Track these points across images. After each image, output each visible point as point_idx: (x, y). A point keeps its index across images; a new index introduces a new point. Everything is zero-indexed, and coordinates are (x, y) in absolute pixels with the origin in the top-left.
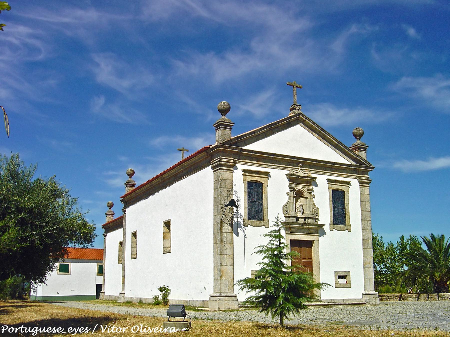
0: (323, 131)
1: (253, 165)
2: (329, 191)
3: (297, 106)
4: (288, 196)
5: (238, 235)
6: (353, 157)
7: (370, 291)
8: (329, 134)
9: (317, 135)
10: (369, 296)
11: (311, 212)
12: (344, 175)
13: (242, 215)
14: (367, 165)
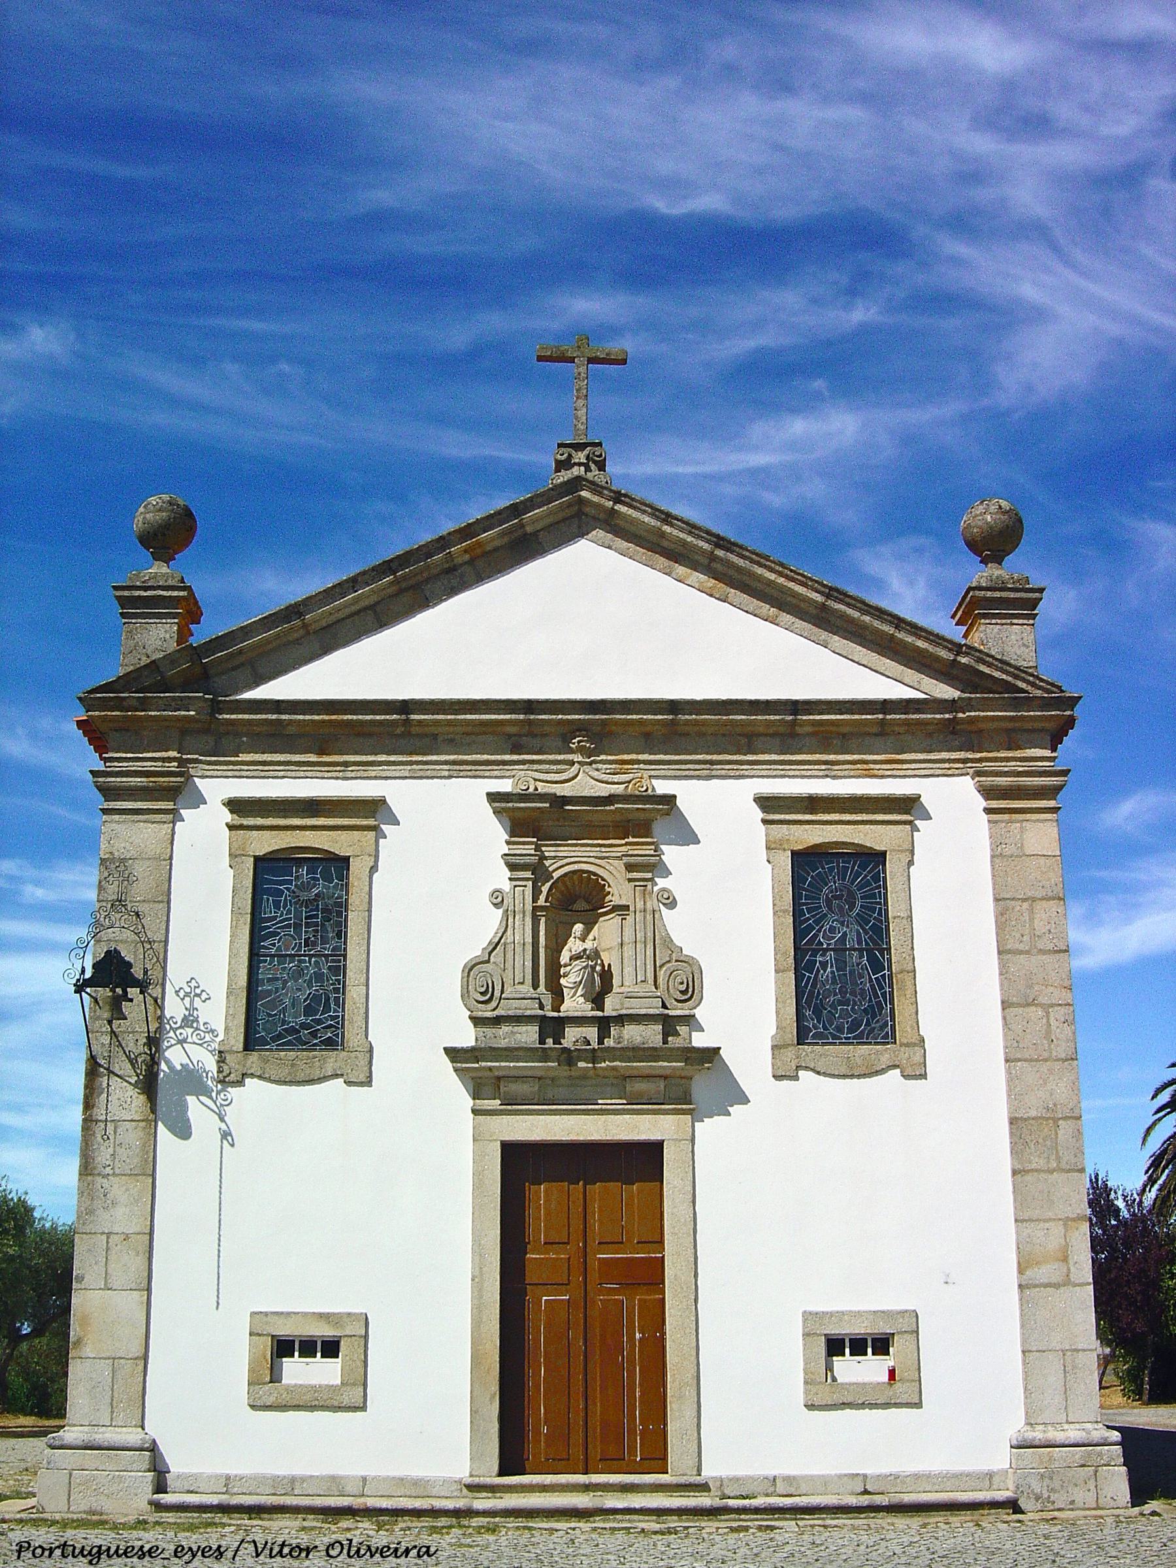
0: (728, 550)
1: (293, 774)
2: (769, 861)
3: (579, 447)
4: (501, 911)
5: (183, 1131)
6: (938, 659)
7: (1066, 1426)
8: (761, 559)
9: (698, 577)
10: (1051, 1459)
11: (644, 985)
12: (878, 766)
13: (212, 1031)
14: (1029, 688)
